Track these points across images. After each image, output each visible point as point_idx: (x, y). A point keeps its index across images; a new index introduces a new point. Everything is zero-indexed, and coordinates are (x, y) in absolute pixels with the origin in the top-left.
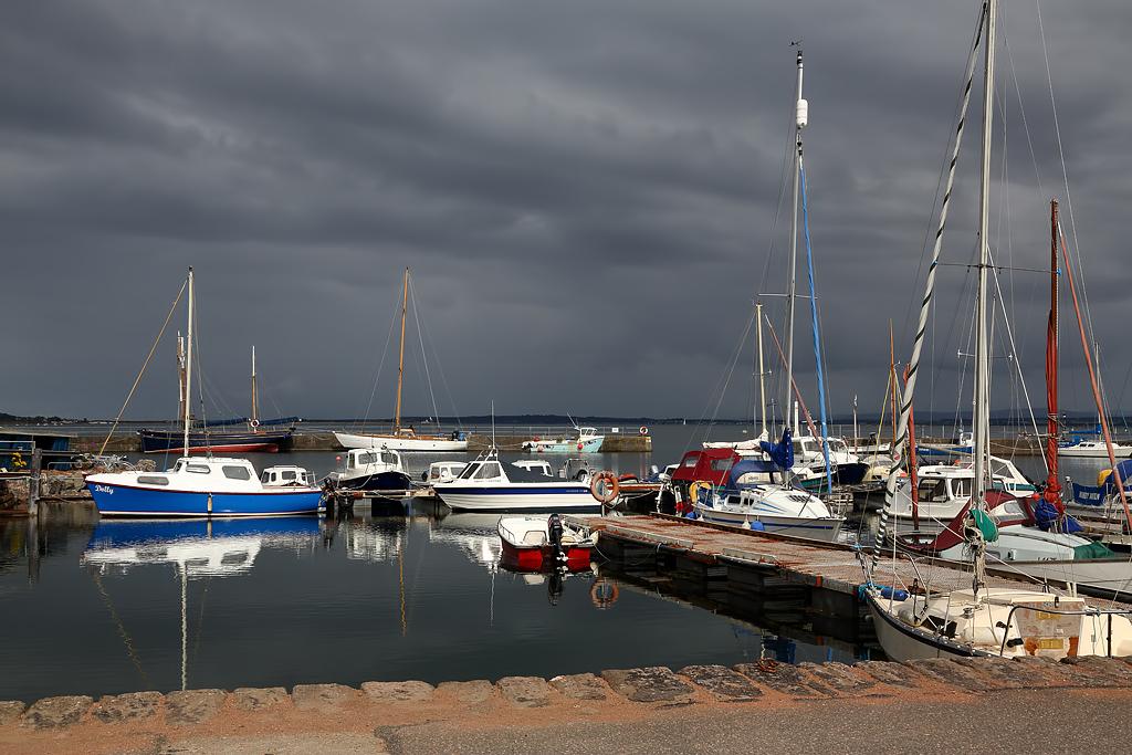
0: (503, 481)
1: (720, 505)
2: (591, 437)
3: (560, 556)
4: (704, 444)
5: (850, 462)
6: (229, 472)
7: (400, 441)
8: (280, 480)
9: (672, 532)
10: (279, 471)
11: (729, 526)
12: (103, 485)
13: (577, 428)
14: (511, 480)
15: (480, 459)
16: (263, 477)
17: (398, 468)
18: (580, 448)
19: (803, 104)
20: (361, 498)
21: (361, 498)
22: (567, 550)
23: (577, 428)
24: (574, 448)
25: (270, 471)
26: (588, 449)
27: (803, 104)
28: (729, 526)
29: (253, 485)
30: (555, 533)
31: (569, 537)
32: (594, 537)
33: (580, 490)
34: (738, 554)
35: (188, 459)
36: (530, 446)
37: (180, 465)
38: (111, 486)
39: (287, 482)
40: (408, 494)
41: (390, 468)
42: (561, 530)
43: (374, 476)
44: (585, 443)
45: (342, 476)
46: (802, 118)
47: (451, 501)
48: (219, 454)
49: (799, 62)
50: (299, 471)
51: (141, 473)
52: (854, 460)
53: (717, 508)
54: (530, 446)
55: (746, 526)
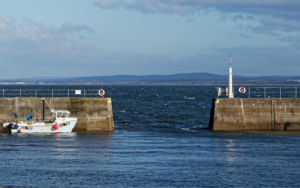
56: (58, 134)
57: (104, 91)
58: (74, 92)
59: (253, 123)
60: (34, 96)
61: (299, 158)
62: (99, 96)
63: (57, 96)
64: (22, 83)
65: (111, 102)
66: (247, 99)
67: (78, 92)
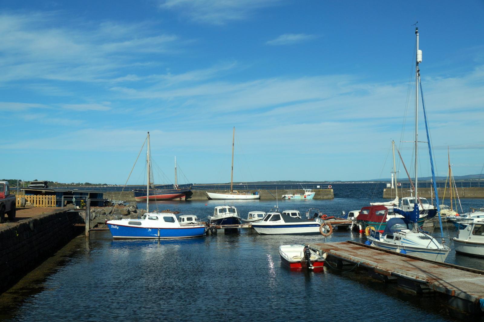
0: (282, 222)
1: (383, 239)
2: (310, 193)
3: (310, 266)
4: (371, 204)
5: (430, 208)
6: (167, 220)
7: (233, 195)
8: (186, 221)
9: (361, 253)
10: (185, 217)
11: (388, 251)
12: (114, 225)
13: (304, 189)
14: (286, 222)
15: (271, 212)
16: (180, 220)
17: (235, 215)
18: (305, 197)
19: (420, 52)
20: (220, 228)
21: (220, 228)
22: (315, 263)
23: (304, 189)
24: (303, 198)
25: (182, 217)
26: (308, 198)
27: (420, 52)
28: (388, 251)
29: (176, 225)
30: (307, 255)
31: (314, 257)
32: (325, 256)
33: (316, 225)
34: (403, 272)
35: (149, 214)
36: (285, 197)
37: (145, 216)
38: (118, 225)
39: (189, 222)
40: (240, 226)
41: (231, 215)
42: (310, 254)
43: (225, 218)
44: (307, 195)
45: (213, 218)
46: (420, 58)
47: (259, 230)
48: (161, 211)
49: (416, 33)
50: (194, 217)
51: (129, 220)
52: (432, 207)
53: (382, 240)
54: (285, 197)
55: (398, 251)
56: (307, 200)
57: (331, 186)
58: (317, 187)
59: (23, 277)
60: (291, 189)
61: (479, 193)
62: (329, 188)
63: (324, 188)
64: (372, 182)
65: (333, 191)
66: (478, 188)
67: (318, 187)
